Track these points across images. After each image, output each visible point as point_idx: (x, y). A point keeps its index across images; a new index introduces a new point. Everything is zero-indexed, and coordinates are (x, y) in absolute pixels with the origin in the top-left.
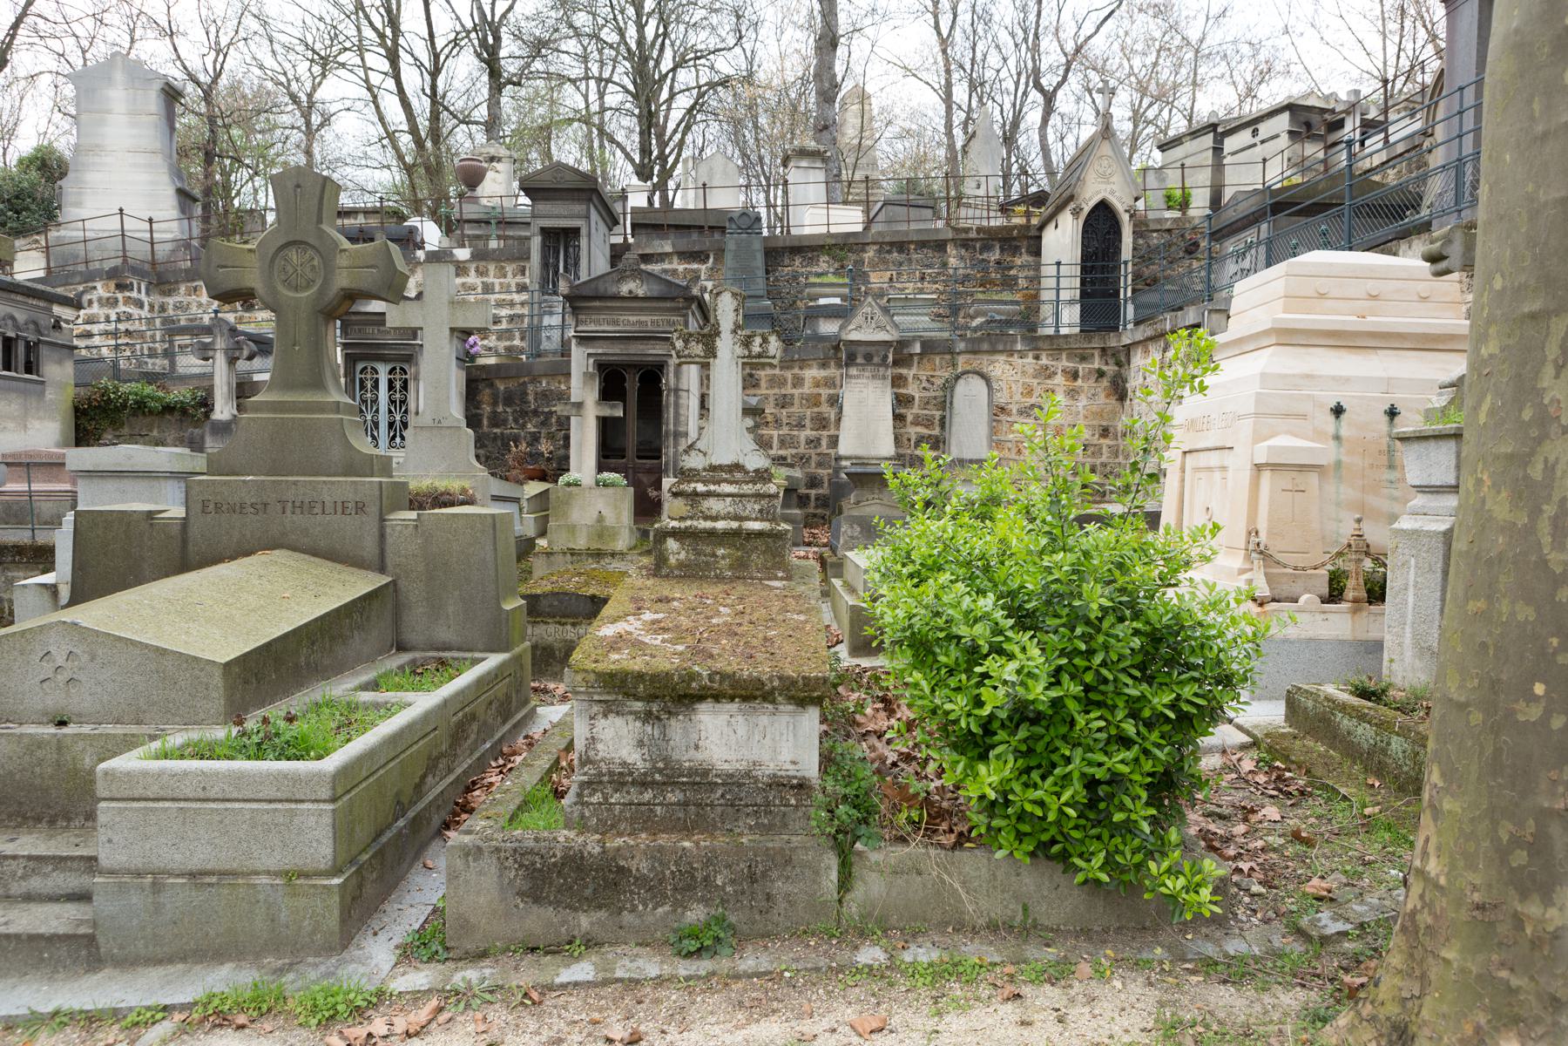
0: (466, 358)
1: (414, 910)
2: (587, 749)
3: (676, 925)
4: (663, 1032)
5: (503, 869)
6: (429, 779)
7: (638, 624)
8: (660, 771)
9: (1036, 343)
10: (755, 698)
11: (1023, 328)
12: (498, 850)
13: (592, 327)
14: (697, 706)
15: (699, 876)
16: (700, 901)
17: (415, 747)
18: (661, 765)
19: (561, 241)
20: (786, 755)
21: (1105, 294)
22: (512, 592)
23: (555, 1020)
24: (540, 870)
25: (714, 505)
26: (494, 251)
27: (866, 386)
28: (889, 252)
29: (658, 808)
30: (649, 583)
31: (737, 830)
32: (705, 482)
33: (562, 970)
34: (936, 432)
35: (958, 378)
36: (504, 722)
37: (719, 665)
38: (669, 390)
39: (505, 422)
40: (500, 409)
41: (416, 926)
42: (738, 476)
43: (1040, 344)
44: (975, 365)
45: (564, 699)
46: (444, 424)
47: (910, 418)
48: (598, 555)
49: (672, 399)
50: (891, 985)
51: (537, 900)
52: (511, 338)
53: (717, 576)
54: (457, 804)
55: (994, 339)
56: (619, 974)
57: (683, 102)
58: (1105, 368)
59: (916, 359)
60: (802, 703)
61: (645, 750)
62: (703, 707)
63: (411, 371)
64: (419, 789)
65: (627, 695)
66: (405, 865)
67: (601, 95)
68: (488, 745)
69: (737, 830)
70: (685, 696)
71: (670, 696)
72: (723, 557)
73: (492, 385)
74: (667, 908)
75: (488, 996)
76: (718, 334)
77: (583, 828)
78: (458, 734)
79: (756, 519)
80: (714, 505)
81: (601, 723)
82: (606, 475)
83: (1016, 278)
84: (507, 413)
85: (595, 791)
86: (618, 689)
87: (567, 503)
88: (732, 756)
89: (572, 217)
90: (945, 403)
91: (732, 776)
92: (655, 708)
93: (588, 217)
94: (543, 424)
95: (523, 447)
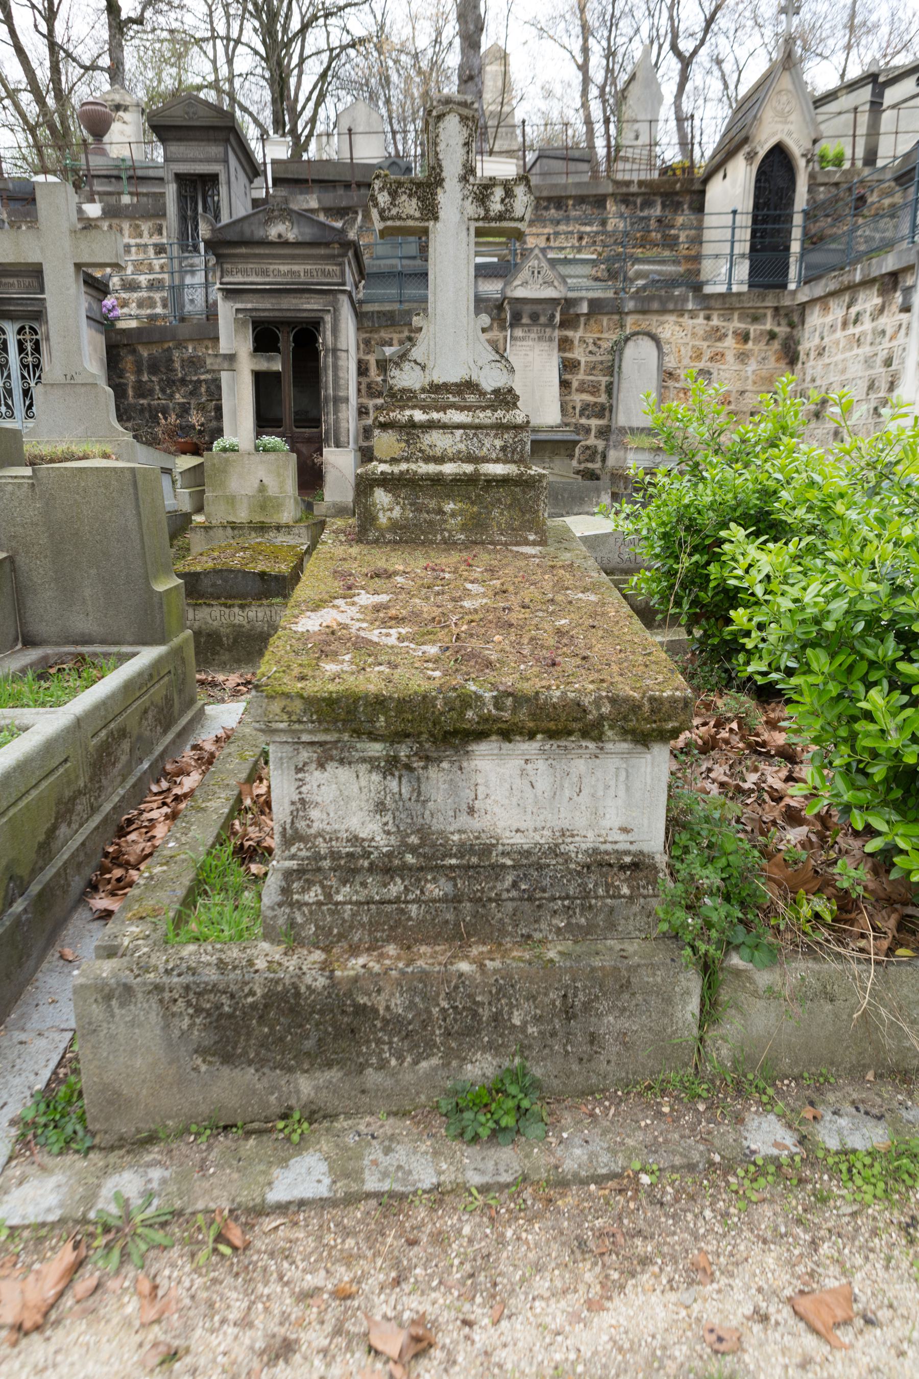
0: (104, 323)
1: (42, 1043)
2: (294, 816)
3: (449, 1084)
4: (466, 1323)
5: (168, 1016)
6: (63, 830)
7: (353, 611)
8: (413, 850)
9: (708, 303)
10: (570, 733)
11: (685, 288)
12: (158, 988)
13: (239, 278)
14: (473, 747)
15: (485, 1013)
16: (486, 1049)
17: (34, 793)
18: (414, 840)
19: (197, 188)
20: (612, 819)
21: (775, 248)
22: (165, 570)
23: (275, 1288)
24: (231, 1016)
25: (439, 441)
26: (127, 206)
27: (532, 349)
28: (546, 208)
29: (413, 908)
30: (354, 550)
31: (537, 936)
32: (425, 409)
33: (276, 1172)
34: (603, 399)
35: (627, 339)
36: (165, 732)
37: (508, 681)
38: (327, 351)
39: (151, 392)
40: (145, 378)
41: (40, 1086)
42: (471, 398)
43: (713, 303)
44: (644, 326)
45: (236, 694)
46: (79, 380)
47: (575, 384)
48: (262, 528)
49: (330, 360)
50: (823, 1199)
51: (228, 1059)
52: (152, 305)
53: (445, 541)
54: (106, 855)
55: (663, 297)
56: (372, 1184)
57: (313, 68)
58: (777, 329)
59: (582, 319)
60: (643, 739)
61: (388, 818)
62: (481, 748)
63: (42, 330)
64: (46, 849)
65: (357, 733)
66: (31, 963)
67: (230, 62)
68: (146, 765)
69: (537, 936)
70: (455, 733)
71: (427, 732)
72: (453, 515)
73: (134, 352)
74: (435, 1061)
75: (158, 1236)
76: (440, 182)
77: (293, 938)
78: (101, 761)
79: (497, 461)
80: (439, 441)
81: (315, 777)
82: (266, 439)
83: (677, 237)
84: (152, 379)
85: (310, 883)
86: (342, 723)
87: (225, 471)
88: (527, 823)
89: (208, 161)
90: (612, 369)
91: (528, 853)
92: (403, 752)
93: (226, 161)
94: (192, 393)
95: (172, 419)
